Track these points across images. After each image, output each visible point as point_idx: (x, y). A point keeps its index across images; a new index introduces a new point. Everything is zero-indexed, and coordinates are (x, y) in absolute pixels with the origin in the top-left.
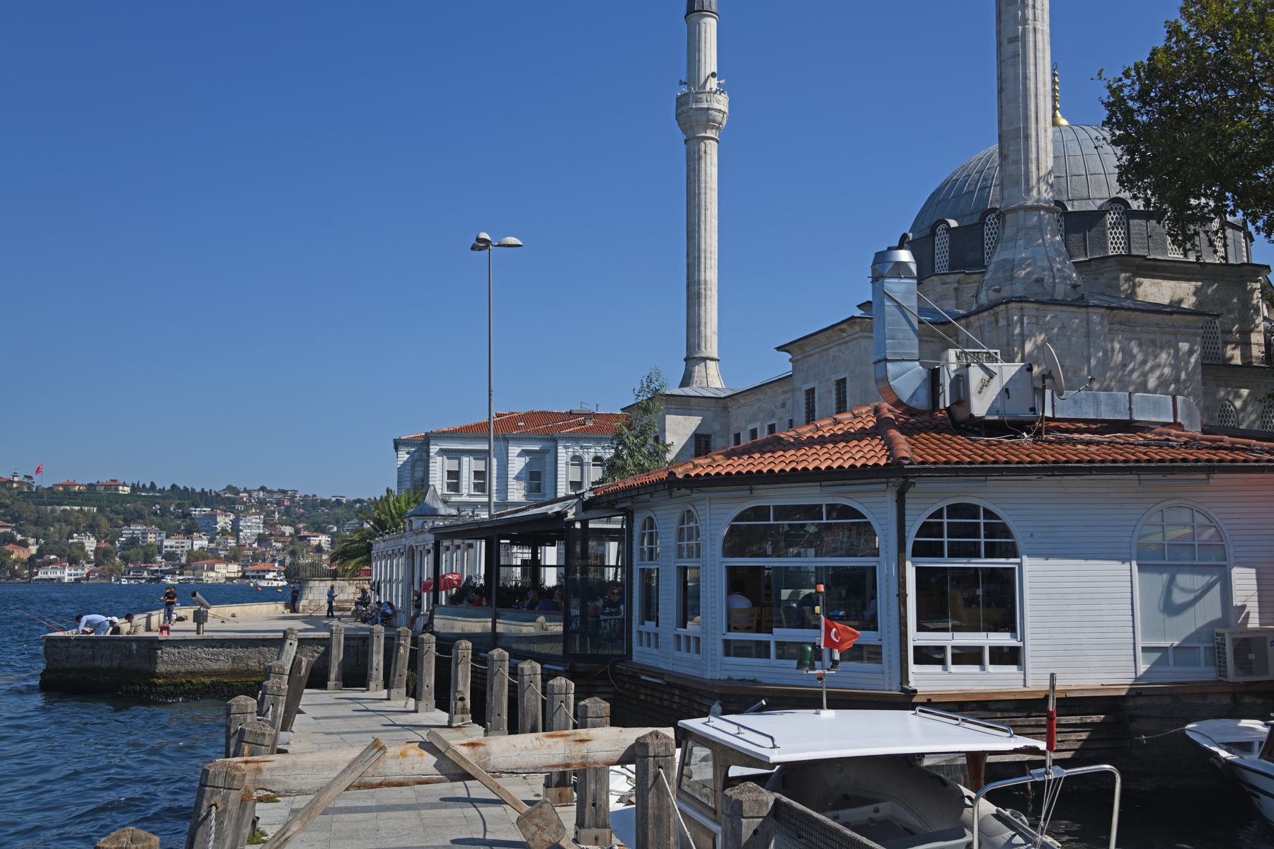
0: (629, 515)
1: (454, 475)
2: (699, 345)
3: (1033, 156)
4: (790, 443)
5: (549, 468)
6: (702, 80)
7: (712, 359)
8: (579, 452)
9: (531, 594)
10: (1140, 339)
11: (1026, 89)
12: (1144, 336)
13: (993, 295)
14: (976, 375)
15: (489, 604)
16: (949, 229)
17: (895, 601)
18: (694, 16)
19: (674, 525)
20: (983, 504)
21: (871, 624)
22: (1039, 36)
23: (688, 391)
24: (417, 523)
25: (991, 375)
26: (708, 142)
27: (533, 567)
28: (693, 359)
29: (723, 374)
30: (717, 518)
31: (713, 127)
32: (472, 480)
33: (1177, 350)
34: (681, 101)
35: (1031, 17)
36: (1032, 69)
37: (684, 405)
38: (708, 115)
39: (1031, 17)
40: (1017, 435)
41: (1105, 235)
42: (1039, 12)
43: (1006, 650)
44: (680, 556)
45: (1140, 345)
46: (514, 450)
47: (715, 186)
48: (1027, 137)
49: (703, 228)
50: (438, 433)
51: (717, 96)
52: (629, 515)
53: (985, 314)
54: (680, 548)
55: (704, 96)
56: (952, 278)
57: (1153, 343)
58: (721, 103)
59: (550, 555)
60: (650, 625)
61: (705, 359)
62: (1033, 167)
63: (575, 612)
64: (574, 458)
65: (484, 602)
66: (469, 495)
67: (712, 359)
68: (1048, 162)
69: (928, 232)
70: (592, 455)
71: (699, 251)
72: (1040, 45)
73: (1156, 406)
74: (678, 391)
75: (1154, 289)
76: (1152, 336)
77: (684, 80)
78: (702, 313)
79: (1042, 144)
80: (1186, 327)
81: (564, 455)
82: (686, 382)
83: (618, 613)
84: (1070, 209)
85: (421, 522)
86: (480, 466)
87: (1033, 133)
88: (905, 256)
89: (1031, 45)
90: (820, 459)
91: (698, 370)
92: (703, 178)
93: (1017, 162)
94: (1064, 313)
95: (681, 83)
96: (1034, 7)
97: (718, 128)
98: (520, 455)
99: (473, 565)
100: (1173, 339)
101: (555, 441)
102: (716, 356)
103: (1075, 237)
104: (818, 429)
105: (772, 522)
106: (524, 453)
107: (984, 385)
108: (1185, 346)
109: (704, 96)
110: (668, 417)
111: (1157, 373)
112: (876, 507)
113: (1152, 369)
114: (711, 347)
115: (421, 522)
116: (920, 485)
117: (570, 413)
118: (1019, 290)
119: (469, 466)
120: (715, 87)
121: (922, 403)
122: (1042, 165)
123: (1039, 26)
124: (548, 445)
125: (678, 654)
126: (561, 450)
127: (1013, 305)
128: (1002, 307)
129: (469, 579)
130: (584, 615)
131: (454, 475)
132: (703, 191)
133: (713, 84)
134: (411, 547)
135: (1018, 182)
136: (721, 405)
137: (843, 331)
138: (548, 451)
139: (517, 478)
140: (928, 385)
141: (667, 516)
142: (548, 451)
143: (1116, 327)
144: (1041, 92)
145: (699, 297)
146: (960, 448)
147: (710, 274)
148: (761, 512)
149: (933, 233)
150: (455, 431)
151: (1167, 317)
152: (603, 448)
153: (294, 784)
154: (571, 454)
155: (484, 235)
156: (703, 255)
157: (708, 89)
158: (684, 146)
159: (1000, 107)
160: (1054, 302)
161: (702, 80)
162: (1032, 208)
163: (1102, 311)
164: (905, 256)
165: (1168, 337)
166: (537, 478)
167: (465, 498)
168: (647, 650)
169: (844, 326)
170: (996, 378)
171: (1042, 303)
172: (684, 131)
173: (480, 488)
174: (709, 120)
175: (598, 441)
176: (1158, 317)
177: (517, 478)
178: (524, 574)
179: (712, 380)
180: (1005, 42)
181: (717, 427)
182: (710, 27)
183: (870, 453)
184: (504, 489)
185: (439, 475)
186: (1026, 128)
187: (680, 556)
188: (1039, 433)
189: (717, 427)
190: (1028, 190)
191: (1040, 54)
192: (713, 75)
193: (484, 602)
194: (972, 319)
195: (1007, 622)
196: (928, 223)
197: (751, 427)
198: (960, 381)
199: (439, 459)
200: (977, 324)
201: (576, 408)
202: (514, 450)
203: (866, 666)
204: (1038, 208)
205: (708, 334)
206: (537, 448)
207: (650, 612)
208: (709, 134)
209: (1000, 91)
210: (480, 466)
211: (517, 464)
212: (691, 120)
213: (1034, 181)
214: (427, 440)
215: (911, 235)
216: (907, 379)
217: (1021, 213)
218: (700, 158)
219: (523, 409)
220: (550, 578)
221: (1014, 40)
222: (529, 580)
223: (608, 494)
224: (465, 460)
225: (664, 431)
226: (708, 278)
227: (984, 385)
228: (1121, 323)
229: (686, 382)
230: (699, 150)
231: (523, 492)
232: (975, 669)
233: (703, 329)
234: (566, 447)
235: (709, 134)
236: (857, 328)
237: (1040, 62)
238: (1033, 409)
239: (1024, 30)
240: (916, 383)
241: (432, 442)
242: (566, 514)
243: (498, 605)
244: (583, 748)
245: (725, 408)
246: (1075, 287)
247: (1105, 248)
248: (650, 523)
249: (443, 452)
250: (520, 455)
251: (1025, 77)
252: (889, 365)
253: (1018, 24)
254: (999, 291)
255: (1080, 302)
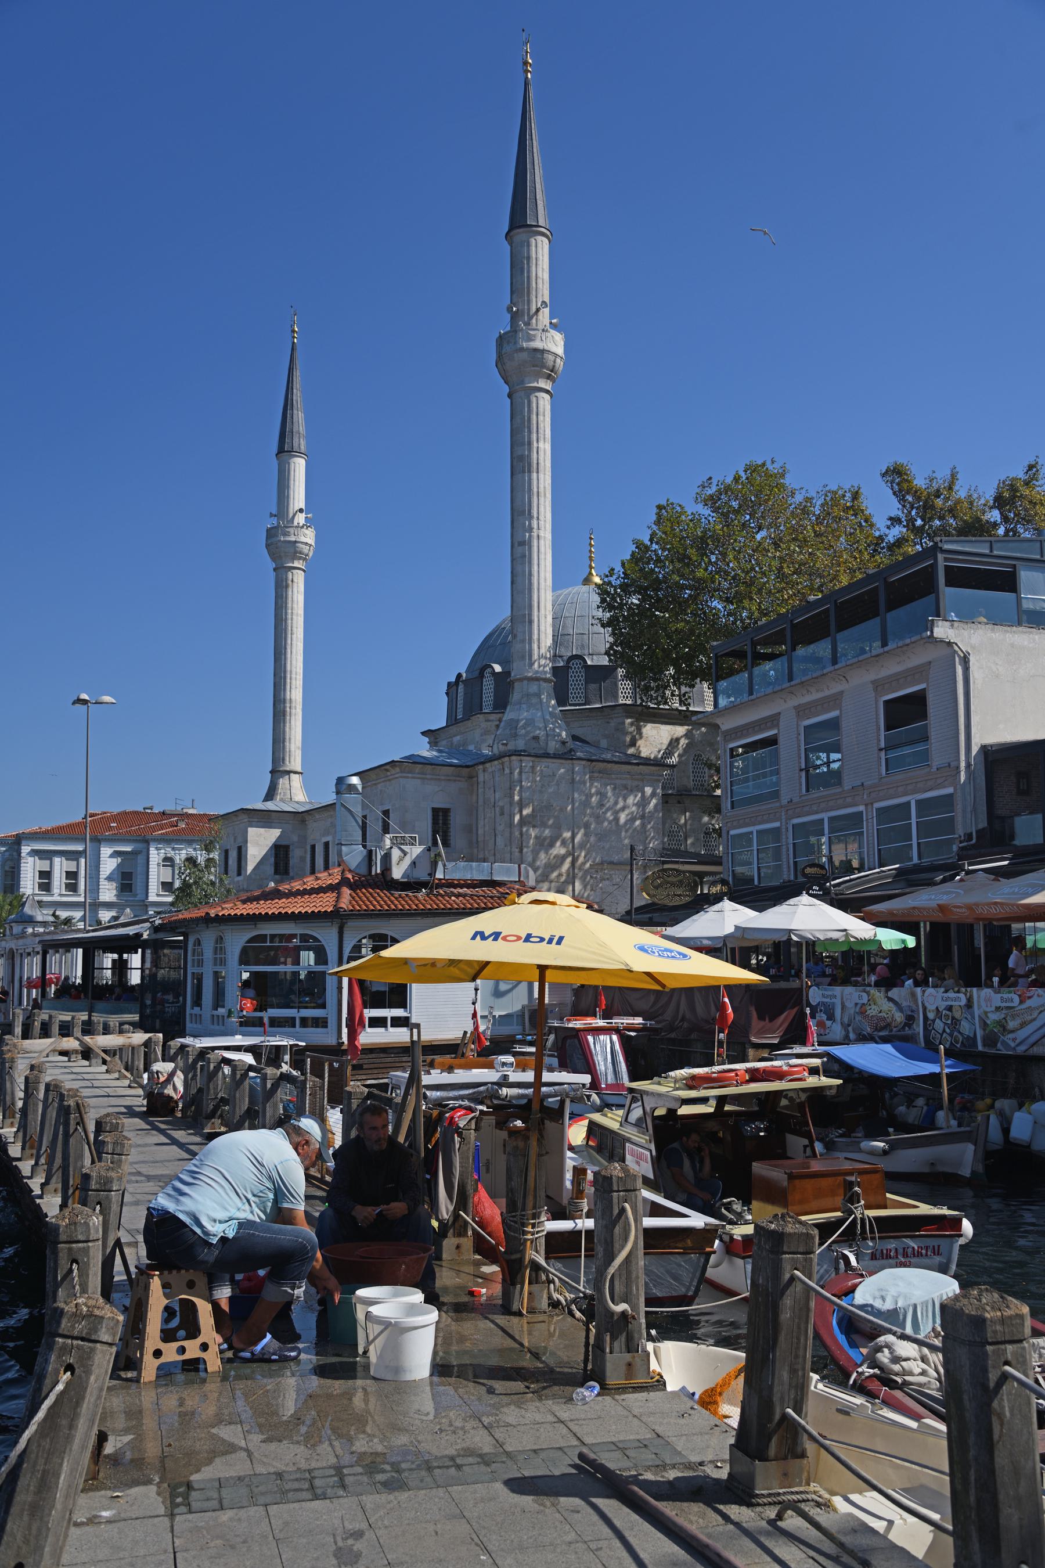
0: (186, 935)
1: (46, 875)
2: (284, 759)
3: (535, 637)
4: (285, 893)
5: (140, 869)
6: (291, 515)
7: (296, 773)
8: (171, 853)
9: (117, 990)
10: (615, 784)
11: (530, 584)
12: (618, 782)
13: (502, 748)
14: (396, 853)
15: (86, 996)
16: (494, 673)
17: (335, 991)
18: (284, 455)
19: (212, 944)
20: (390, 933)
21: (323, 1006)
22: (542, 542)
23: (270, 806)
24: (17, 929)
25: (405, 853)
26: (295, 571)
27: (121, 968)
28: (278, 772)
29: (307, 786)
30: (237, 940)
31: (300, 558)
32: (64, 880)
33: (643, 793)
34: (271, 533)
35: (535, 526)
36: (535, 568)
37: (264, 818)
38: (296, 547)
39: (535, 526)
40: (419, 890)
41: (616, 685)
42: (542, 523)
43: (866, 1075)
44: (215, 965)
45: (614, 789)
46: (106, 851)
47: (301, 612)
48: (531, 622)
49: (289, 651)
50: (30, 833)
51: (304, 530)
52: (186, 935)
53: (496, 762)
54: (216, 959)
55: (292, 530)
56: (493, 717)
57: (625, 787)
58: (308, 537)
59: (135, 960)
60: (197, 1009)
61: (289, 772)
62: (535, 646)
63: (149, 1002)
64: (166, 859)
65: (82, 996)
66: (61, 895)
67: (296, 773)
68: (547, 641)
69: (477, 673)
70: (184, 856)
71: (285, 672)
72: (542, 549)
73: (508, 871)
74: (260, 806)
75: (654, 732)
76: (624, 782)
77: (274, 513)
78: (287, 729)
79: (542, 628)
80: (650, 775)
81: (155, 856)
82: (270, 796)
83: (178, 1002)
84: (589, 663)
85: (21, 927)
86: (71, 866)
87: (536, 619)
88: (355, 780)
89: (535, 549)
90: (297, 906)
91: (283, 782)
92: (289, 605)
93: (523, 641)
94: (553, 764)
95: (272, 515)
96: (538, 518)
97: (305, 559)
98: (111, 856)
99: (73, 964)
100: (640, 783)
101: (147, 842)
102: (299, 769)
103: (593, 686)
104: (305, 884)
105: (825, 816)
106: (116, 854)
107: (401, 859)
108: (648, 790)
109: (292, 530)
110: (250, 829)
111: (627, 812)
112: (328, 936)
113: (623, 809)
114: (295, 760)
115: (21, 927)
116: (350, 924)
117: (163, 813)
118: (520, 744)
119: (60, 867)
120: (302, 522)
121: (363, 871)
122: (542, 645)
123: (542, 534)
124: (140, 846)
125: (212, 1027)
126: (153, 851)
127: (514, 758)
128: (507, 759)
129: (67, 978)
130: (154, 1004)
131: (46, 875)
132: (289, 616)
133: (300, 519)
134: (11, 950)
135: (523, 658)
136: (301, 818)
137: (387, 770)
138: (140, 852)
139: (109, 879)
140: (367, 859)
141: (208, 938)
142: (140, 852)
143: (596, 775)
144: (542, 586)
145: (284, 715)
146: (380, 900)
147: (296, 693)
148: (262, 938)
149: (481, 676)
150: (47, 832)
151: (636, 767)
152: (195, 849)
153: (33, 1049)
154: (162, 856)
155: (84, 696)
156: (288, 676)
157: (296, 524)
158: (273, 574)
159: (512, 595)
160: (546, 755)
161: (291, 515)
162: (531, 679)
163: (584, 762)
164: (355, 780)
165: (636, 783)
166: (129, 881)
167: (56, 898)
168: (195, 1026)
169: (387, 767)
170: (408, 856)
171: (536, 756)
172: (273, 559)
173: (72, 888)
174: (296, 552)
175: (190, 842)
176: (629, 767)
177: (109, 879)
178: (113, 974)
179: (296, 793)
180: (516, 545)
181: (295, 838)
182: (299, 466)
183: (325, 903)
184: (94, 887)
185: (30, 875)
186: (530, 615)
187: (215, 965)
188: (431, 889)
189: (295, 838)
190: (531, 664)
191: (542, 556)
192: (301, 511)
193: (82, 996)
194: (488, 765)
195: (403, 1004)
196: (479, 666)
197: (325, 840)
198: (387, 857)
199: (31, 859)
200: (490, 770)
201: (170, 808)
202: (106, 851)
203: (319, 1030)
204: (537, 679)
205: (293, 749)
206: (128, 849)
207: (198, 1002)
208: (296, 564)
209: (512, 583)
210: (71, 866)
211: (109, 865)
212: (280, 551)
213: (536, 657)
214: (17, 841)
215: (464, 675)
216: (354, 855)
217: (525, 682)
218: (287, 586)
219: (116, 810)
220: (135, 978)
221: (522, 543)
222: (116, 979)
223: (170, 922)
224: (57, 860)
225: (246, 842)
226: (293, 698)
227: (401, 859)
228: (600, 772)
229: (270, 796)
230: (287, 579)
231: (115, 892)
232: (383, 1030)
233: (287, 744)
234: (157, 849)
235: (296, 564)
236: (398, 769)
237: (542, 563)
238: (430, 874)
239: (530, 536)
240: (359, 859)
241: (23, 843)
242: (142, 935)
243: (93, 998)
244: (130, 1040)
245: (303, 821)
246: (564, 743)
247: (616, 697)
248: (198, 942)
249: (34, 853)
250: (111, 856)
251: (530, 574)
252: (343, 848)
253: (526, 531)
254: (506, 745)
255: (566, 755)
